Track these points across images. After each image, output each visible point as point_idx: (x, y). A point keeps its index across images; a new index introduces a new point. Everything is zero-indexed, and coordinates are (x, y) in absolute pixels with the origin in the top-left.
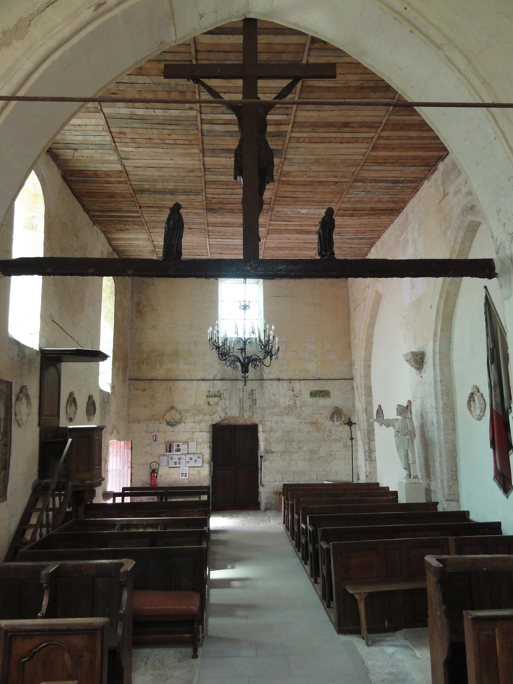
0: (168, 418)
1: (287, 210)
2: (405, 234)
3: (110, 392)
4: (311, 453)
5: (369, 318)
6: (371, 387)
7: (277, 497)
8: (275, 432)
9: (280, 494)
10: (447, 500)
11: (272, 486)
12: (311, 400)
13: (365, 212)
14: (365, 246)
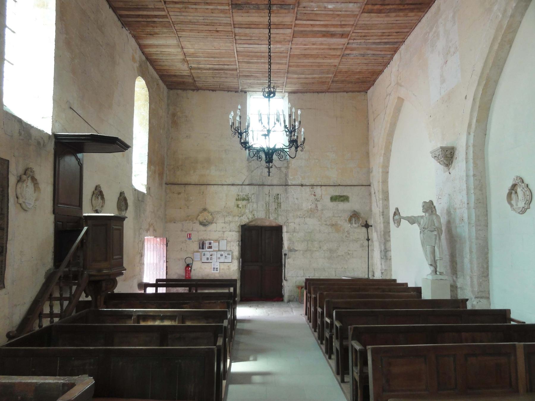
0: (201, 218)
1: (313, 4)
2: (435, 28)
3: (145, 192)
5: (389, 125)
6: (388, 192)
7: (299, 291)
8: (298, 232)
9: (302, 288)
10: (476, 298)
13: (394, 6)
14: (389, 53)
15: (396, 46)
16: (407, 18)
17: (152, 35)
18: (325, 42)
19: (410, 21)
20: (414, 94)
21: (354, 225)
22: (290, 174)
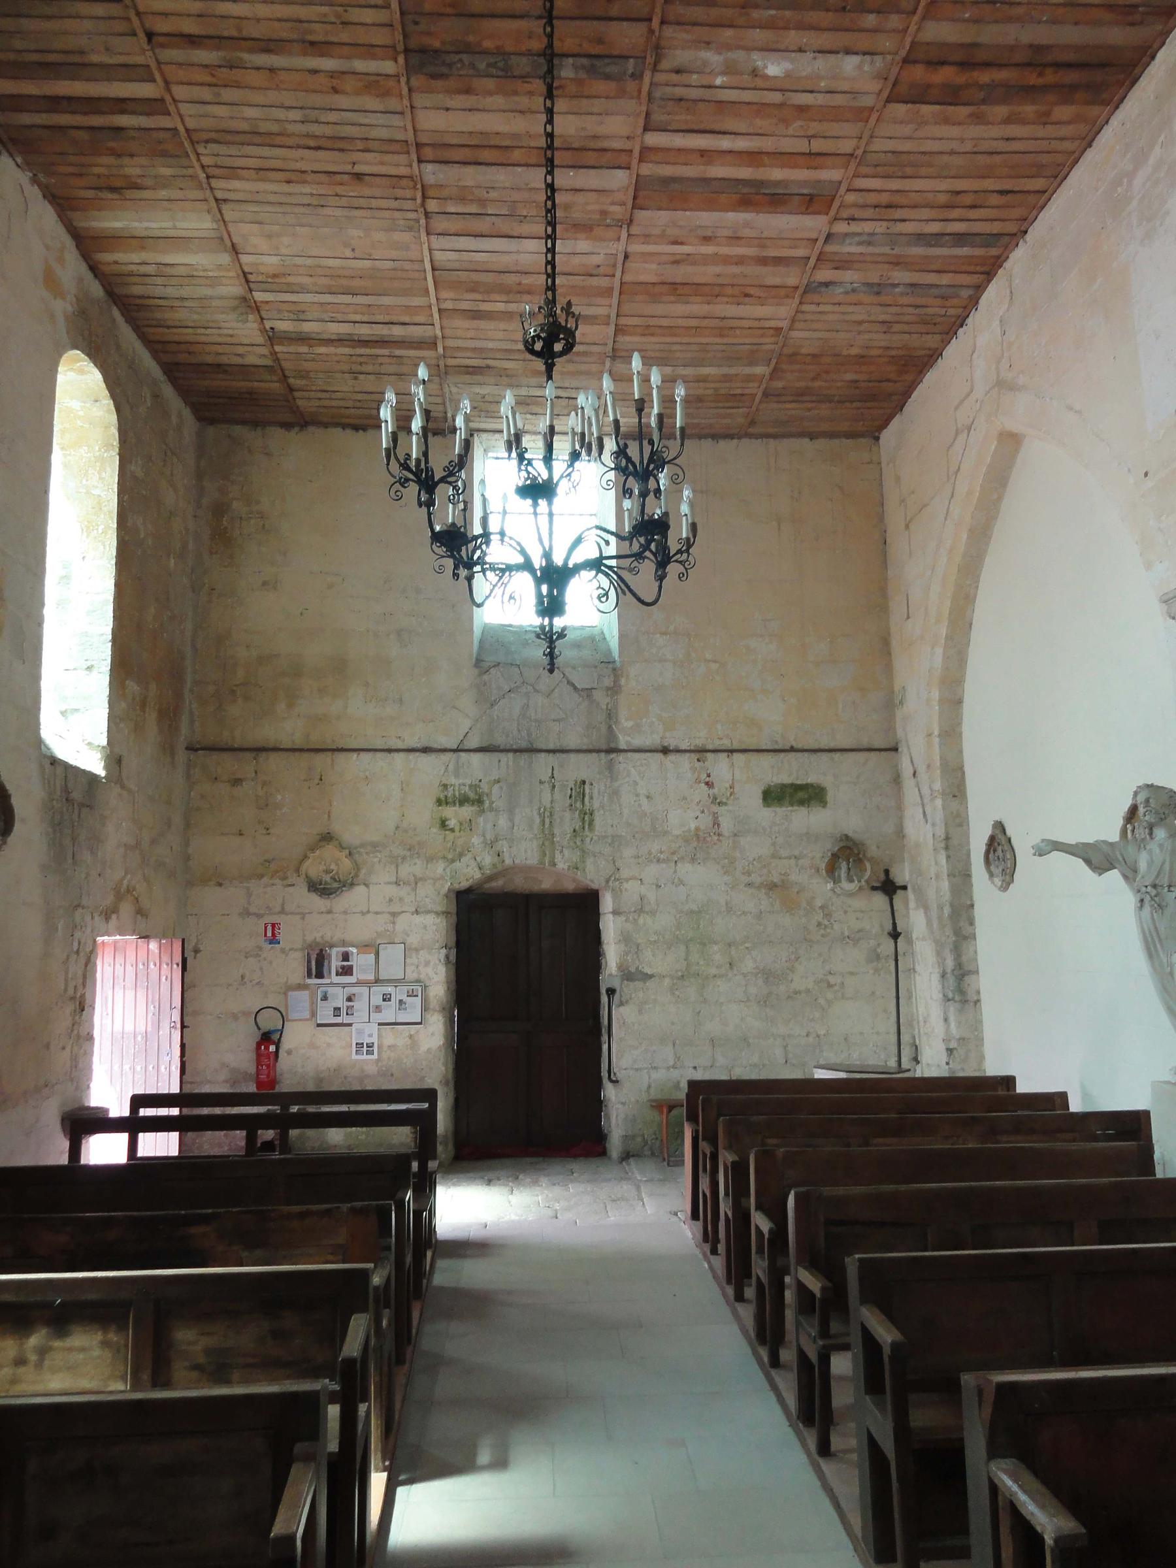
0: (313, 868)
1: (713, 58)
3: (102, 773)
4: (766, 981)
5: (964, 536)
6: (961, 769)
8: (653, 913)
11: (645, 1085)
12: (766, 815)
15: (994, 252)
16: (1050, 131)
17: (121, 189)
18: (747, 232)
19: (1055, 145)
20: (1070, 408)
21: (846, 885)
22: (623, 714)
